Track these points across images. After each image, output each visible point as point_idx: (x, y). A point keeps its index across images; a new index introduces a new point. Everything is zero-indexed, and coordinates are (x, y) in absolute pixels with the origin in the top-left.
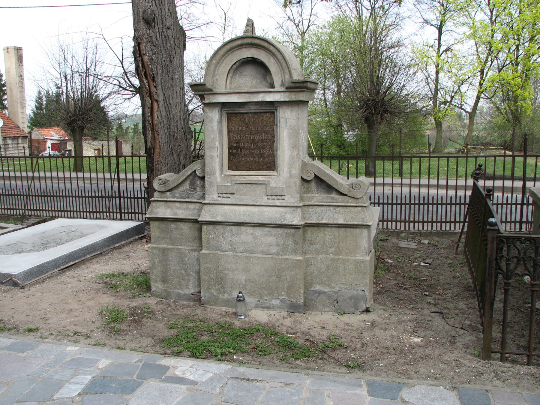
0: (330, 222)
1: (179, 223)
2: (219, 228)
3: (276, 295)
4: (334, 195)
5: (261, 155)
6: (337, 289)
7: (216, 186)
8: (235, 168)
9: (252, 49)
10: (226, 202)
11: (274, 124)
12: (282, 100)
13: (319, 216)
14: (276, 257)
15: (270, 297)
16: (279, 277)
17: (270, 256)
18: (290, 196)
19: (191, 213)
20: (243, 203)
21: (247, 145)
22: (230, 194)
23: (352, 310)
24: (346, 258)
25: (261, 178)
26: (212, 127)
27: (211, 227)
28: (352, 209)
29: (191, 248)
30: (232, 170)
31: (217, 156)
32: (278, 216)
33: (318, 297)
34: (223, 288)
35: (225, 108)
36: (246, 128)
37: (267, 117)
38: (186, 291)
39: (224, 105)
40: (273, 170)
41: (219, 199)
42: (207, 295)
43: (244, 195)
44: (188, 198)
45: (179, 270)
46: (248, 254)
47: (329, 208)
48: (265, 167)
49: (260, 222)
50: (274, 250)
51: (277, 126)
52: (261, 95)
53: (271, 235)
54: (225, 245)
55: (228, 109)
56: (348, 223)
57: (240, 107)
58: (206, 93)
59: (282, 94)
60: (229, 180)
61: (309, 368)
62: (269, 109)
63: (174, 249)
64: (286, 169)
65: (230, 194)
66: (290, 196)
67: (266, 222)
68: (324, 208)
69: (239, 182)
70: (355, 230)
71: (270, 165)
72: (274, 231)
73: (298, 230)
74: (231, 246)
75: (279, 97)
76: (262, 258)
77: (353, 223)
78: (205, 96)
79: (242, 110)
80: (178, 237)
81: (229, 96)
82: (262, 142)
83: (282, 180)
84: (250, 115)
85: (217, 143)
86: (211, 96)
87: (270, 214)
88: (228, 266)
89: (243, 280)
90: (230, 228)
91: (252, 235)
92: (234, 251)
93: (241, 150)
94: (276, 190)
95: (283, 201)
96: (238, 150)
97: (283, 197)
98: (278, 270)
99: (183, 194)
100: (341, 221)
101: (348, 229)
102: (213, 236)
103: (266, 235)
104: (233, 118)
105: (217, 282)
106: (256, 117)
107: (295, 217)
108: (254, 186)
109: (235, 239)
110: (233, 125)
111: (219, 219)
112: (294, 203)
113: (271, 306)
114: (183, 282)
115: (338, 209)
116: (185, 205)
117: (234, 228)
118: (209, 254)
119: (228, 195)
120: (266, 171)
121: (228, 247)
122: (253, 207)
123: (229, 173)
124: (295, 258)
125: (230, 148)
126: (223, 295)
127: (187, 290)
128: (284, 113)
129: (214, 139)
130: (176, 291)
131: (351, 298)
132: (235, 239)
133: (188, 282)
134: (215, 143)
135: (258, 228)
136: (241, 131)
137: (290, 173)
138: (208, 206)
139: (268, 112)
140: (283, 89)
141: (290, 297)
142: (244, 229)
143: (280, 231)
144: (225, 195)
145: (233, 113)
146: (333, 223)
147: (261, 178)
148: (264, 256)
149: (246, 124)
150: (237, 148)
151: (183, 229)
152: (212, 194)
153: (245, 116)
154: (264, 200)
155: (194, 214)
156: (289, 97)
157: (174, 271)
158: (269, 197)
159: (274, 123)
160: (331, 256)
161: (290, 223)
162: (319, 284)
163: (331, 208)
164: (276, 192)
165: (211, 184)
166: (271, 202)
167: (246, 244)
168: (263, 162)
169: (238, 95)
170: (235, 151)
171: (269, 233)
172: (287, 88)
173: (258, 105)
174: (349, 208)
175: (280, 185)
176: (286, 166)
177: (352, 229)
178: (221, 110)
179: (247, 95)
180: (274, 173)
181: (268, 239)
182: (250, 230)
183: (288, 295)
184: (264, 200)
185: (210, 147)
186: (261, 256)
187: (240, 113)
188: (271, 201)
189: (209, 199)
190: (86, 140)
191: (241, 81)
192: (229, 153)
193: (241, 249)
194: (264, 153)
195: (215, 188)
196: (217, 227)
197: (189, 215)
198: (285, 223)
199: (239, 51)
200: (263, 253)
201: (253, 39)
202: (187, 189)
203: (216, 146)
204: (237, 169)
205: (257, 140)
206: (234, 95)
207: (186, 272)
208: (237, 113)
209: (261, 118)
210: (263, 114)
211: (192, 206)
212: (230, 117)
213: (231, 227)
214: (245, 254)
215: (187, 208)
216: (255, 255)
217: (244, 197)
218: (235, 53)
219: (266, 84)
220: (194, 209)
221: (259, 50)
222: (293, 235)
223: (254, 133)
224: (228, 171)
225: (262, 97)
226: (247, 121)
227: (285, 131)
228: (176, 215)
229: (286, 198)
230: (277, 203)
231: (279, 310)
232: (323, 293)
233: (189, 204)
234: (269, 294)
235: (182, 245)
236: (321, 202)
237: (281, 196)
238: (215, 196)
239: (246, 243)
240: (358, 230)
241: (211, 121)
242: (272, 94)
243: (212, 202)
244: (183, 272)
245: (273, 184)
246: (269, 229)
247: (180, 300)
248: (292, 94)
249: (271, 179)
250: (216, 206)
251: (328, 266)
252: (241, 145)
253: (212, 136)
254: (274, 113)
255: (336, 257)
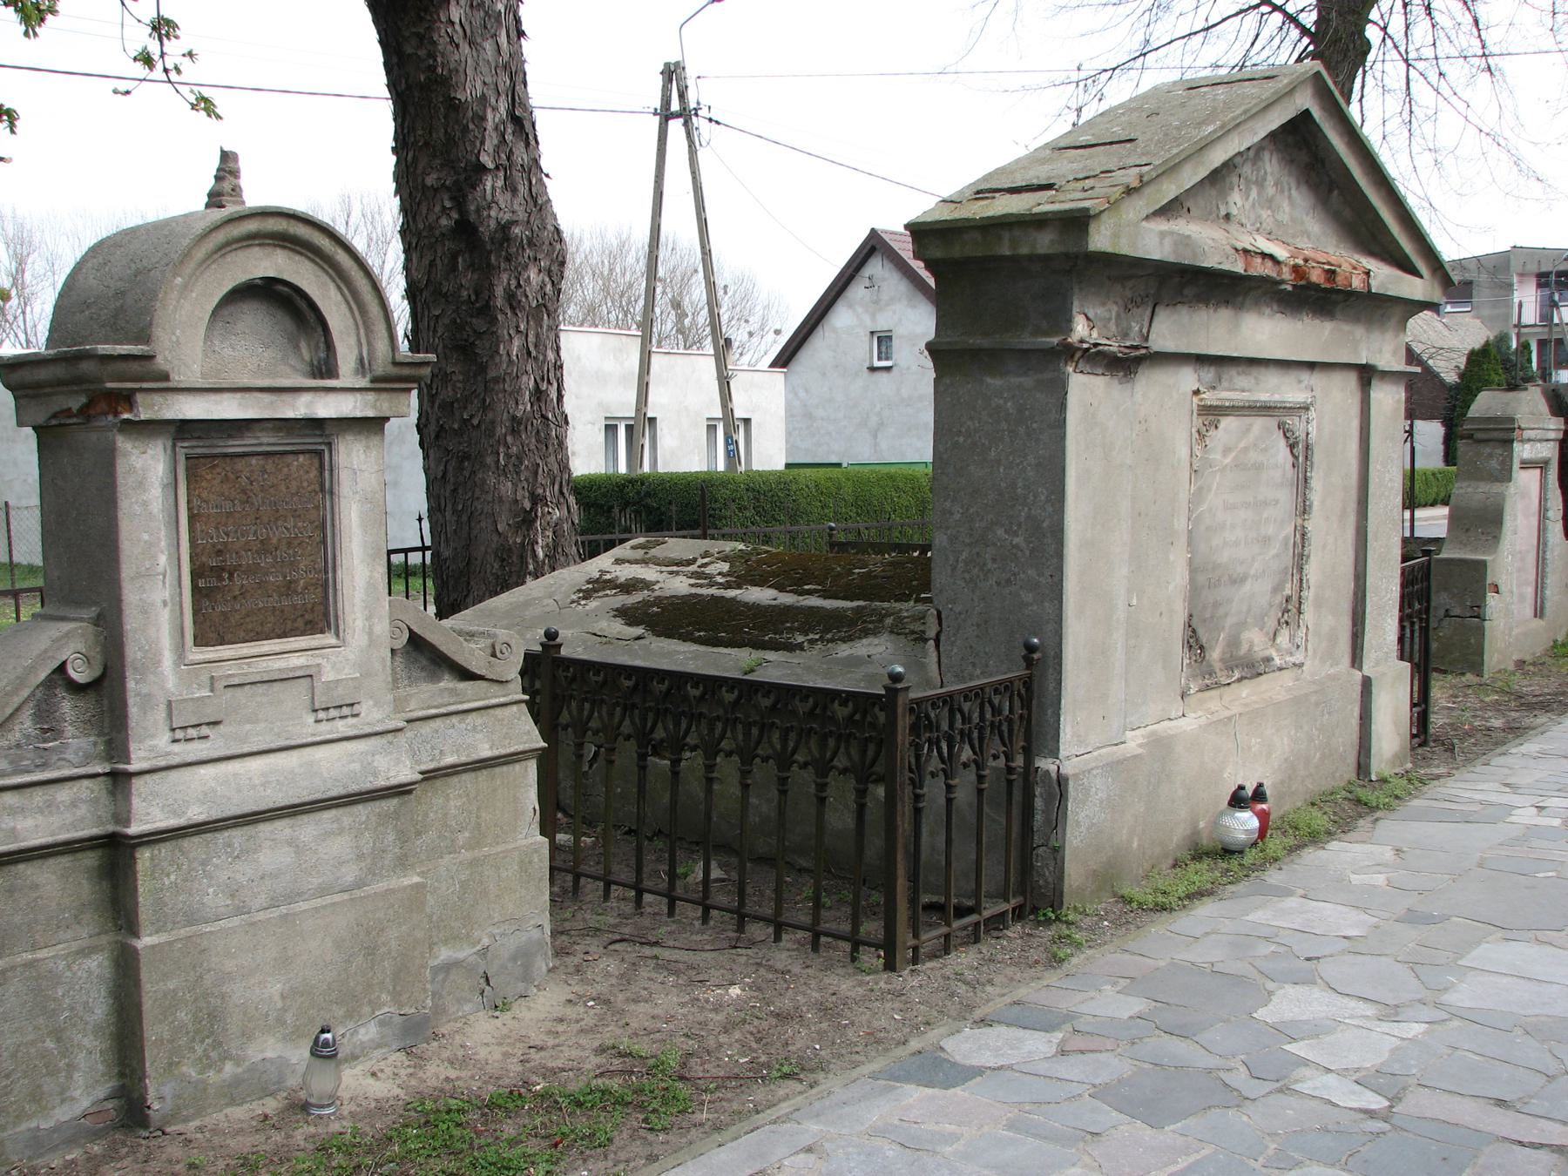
0: (464, 759)
1: (21, 867)
2: (193, 844)
3: (367, 1009)
4: (447, 682)
5: (289, 588)
6: (486, 941)
7: (163, 707)
8: (214, 636)
9: (279, 251)
10: (204, 755)
11: (325, 488)
12: (359, 414)
13: (433, 748)
14: (357, 893)
15: (351, 1025)
16: (371, 951)
17: (346, 896)
18: (371, 703)
19: (68, 817)
20: (246, 749)
21: (247, 559)
22: (208, 724)
23: (521, 986)
24: (499, 849)
25: (297, 661)
26: (145, 504)
27: (164, 850)
28: (498, 711)
29: (75, 946)
30: (206, 645)
31: (165, 603)
32: (356, 766)
33: (444, 980)
34: (217, 1044)
35: (183, 439)
36: (243, 503)
37: (302, 466)
38: (63, 1114)
39: (183, 429)
40: (322, 632)
41: (177, 748)
42: (167, 1090)
43: (249, 721)
44: (44, 766)
45: (33, 1043)
46: (283, 910)
47: (448, 721)
48: (300, 623)
49: (318, 796)
50: (350, 874)
51: (332, 493)
52: (305, 398)
53: (341, 831)
54: (214, 899)
55: (194, 443)
56: (503, 751)
57: (230, 436)
58: (145, 385)
59: (358, 395)
60: (205, 678)
61: (739, 1115)
62: (311, 442)
63: (13, 968)
64: (359, 623)
65: (208, 724)
66: (371, 703)
67: (334, 793)
68: (438, 723)
69: (236, 681)
70: (511, 767)
71: (314, 613)
72: (346, 816)
73: (406, 797)
74: (232, 896)
75: (350, 407)
76: (324, 907)
77: (512, 750)
78: (139, 397)
79: (235, 446)
80: (17, 919)
81: (213, 397)
82: (289, 544)
83: (351, 657)
84: (254, 461)
85: (163, 559)
86: (157, 398)
87: (335, 767)
88: (230, 965)
89: (277, 998)
90: (223, 837)
91: (291, 842)
92: (239, 911)
93: (231, 575)
94: (340, 690)
95: (354, 720)
96: (221, 579)
97: (356, 709)
98: (368, 933)
99: (22, 758)
100: (486, 753)
101: (497, 770)
102: (173, 877)
103: (327, 834)
104: (202, 471)
105: (197, 1032)
106: (270, 467)
107: (398, 762)
108: (277, 686)
109: (243, 872)
110: (205, 495)
111: (197, 813)
112: (382, 721)
113: (357, 1051)
114: (49, 1085)
115: (470, 718)
116: (39, 796)
117: (237, 836)
118: (170, 943)
119: (205, 730)
120: (302, 635)
121: (223, 901)
122: (283, 755)
123: (200, 657)
124: (406, 882)
125: (196, 575)
126: (220, 1071)
127: (66, 1107)
128: (349, 455)
129: (150, 545)
130: (24, 1127)
131: (514, 958)
132: (243, 872)
133: (69, 1077)
134: (154, 557)
135: (305, 818)
136: (229, 515)
137: (370, 633)
138: (147, 777)
139: (302, 452)
140: (363, 382)
141: (401, 1006)
142: (264, 828)
143: (362, 811)
144: (192, 733)
145: (205, 456)
146: (469, 760)
147: (297, 661)
148: (328, 900)
149: (244, 491)
150: (218, 571)
151: (36, 887)
152: (153, 736)
153: (240, 464)
154: (308, 727)
155: (82, 819)
156: (374, 407)
157: (14, 1056)
158: (321, 715)
159: (322, 485)
160: (466, 855)
161: (394, 782)
162: (446, 942)
163: (455, 719)
164: (341, 695)
165: (147, 699)
166: (325, 731)
167: (276, 877)
168: (294, 607)
169: (239, 395)
170: (214, 583)
171: (335, 826)
172: (372, 381)
173: (280, 429)
174: (491, 711)
175: (348, 673)
176: (359, 615)
177: (505, 768)
178: (174, 446)
179: (267, 397)
180: (328, 638)
181: (332, 844)
182: (282, 827)
183: (396, 997)
184: (308, 727)
185: (139, 575)
186: (318, 902)
187: (226, 455)
188: (324, 727)
189: (142, 754)
190: (921, 468)
191: (228, 352)
192: (195, 589)
193: (262, 900)
194: (296, 582)
195: (161, 714)
196: (186, 843)
197: (74, 826)
198: (381, 782)
199: (240, 253)
200: (323, 891)
201: (292, 222)
202: (27, 737)
203: (160, 569)
204: (222, 642)
205: (275, 541)
206: (226, 396)
207: (59, 1040)
208: (215, 456)
209: (285, 470)
210: (290, 458)
211: (64, 794)
212: (195, 468)
213: (226, 834)
214: (274, 913)
215: (50, 805)
216: (303, 906)
217: (248, 727)
218: (229, 258)
219: (299, 366)
220: (74, 804)
221: (297, 258)
222: (396, 815)
223: (266, 519)
224: (194, 649)
225: (308, 406)
226: (243, 481)
227: (354, 507)
228: (16, 839)
229: (364, 709)
230: (342, 728)
231: (378, 1053)
232: (457, 964)
233: (52, 789)
234: (349, 1015)
235: (35, 948)
236: (429, 708)
237: (348, 707)
238: (162, 740)
239: (275, 876)
240: (517, 766)
241: (141, 485)
242: (332, 398)
243: (163, 763)
244: (50, 1044)
245: (328, 675)
246: (333, 812)
247: (41, 1155)
248: (384, 396)
249: (323, 656)
250: (174, 774)
251: (464, 885)
252: (231, 561)
253: (146, 537)
254: (320, 454)
255: (476, 853)
